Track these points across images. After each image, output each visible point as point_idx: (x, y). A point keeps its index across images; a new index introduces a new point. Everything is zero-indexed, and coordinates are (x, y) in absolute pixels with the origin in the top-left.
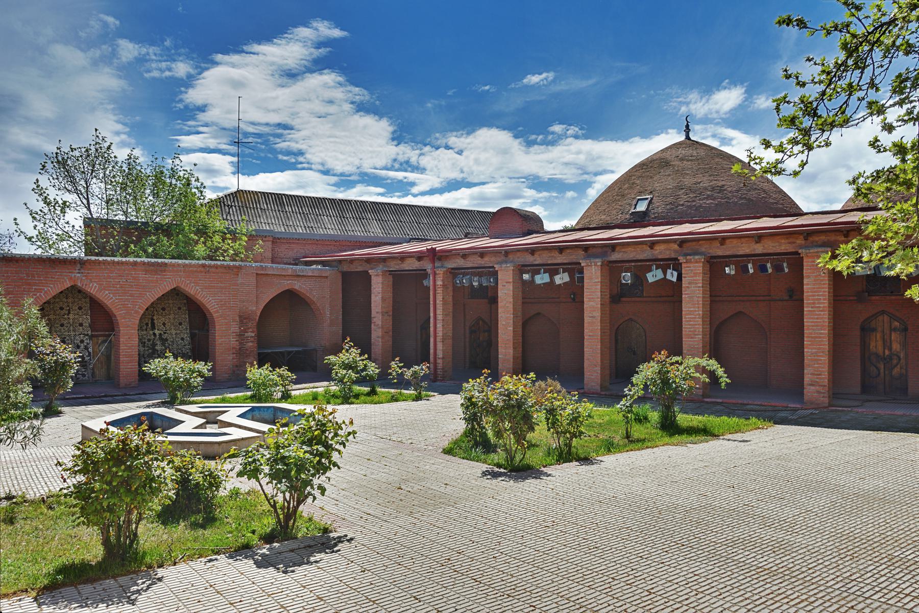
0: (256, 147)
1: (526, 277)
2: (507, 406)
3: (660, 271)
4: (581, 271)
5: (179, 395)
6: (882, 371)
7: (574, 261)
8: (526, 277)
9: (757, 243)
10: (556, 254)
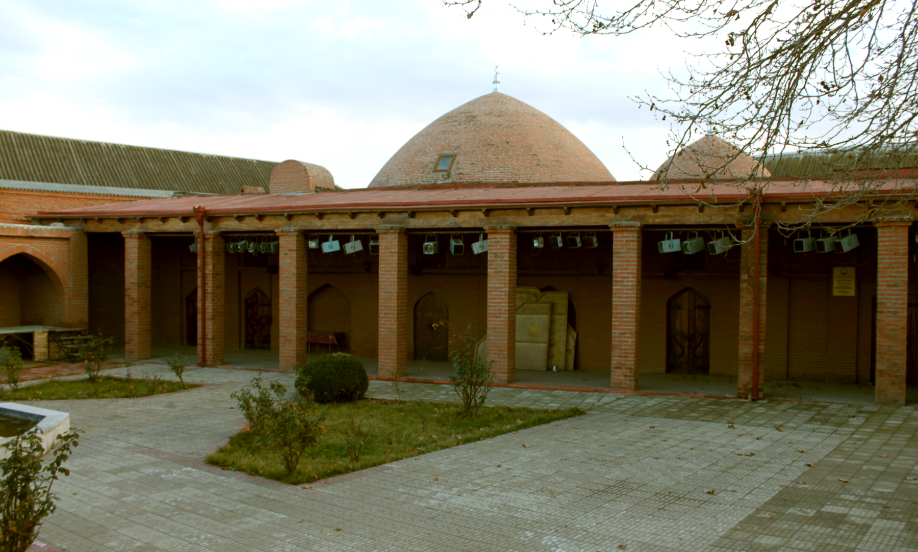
1: (313, 245)
4: (376, 238)
6: (686, 349)
7: (369, 227)
8: (313, 245)
10: (347, 219)
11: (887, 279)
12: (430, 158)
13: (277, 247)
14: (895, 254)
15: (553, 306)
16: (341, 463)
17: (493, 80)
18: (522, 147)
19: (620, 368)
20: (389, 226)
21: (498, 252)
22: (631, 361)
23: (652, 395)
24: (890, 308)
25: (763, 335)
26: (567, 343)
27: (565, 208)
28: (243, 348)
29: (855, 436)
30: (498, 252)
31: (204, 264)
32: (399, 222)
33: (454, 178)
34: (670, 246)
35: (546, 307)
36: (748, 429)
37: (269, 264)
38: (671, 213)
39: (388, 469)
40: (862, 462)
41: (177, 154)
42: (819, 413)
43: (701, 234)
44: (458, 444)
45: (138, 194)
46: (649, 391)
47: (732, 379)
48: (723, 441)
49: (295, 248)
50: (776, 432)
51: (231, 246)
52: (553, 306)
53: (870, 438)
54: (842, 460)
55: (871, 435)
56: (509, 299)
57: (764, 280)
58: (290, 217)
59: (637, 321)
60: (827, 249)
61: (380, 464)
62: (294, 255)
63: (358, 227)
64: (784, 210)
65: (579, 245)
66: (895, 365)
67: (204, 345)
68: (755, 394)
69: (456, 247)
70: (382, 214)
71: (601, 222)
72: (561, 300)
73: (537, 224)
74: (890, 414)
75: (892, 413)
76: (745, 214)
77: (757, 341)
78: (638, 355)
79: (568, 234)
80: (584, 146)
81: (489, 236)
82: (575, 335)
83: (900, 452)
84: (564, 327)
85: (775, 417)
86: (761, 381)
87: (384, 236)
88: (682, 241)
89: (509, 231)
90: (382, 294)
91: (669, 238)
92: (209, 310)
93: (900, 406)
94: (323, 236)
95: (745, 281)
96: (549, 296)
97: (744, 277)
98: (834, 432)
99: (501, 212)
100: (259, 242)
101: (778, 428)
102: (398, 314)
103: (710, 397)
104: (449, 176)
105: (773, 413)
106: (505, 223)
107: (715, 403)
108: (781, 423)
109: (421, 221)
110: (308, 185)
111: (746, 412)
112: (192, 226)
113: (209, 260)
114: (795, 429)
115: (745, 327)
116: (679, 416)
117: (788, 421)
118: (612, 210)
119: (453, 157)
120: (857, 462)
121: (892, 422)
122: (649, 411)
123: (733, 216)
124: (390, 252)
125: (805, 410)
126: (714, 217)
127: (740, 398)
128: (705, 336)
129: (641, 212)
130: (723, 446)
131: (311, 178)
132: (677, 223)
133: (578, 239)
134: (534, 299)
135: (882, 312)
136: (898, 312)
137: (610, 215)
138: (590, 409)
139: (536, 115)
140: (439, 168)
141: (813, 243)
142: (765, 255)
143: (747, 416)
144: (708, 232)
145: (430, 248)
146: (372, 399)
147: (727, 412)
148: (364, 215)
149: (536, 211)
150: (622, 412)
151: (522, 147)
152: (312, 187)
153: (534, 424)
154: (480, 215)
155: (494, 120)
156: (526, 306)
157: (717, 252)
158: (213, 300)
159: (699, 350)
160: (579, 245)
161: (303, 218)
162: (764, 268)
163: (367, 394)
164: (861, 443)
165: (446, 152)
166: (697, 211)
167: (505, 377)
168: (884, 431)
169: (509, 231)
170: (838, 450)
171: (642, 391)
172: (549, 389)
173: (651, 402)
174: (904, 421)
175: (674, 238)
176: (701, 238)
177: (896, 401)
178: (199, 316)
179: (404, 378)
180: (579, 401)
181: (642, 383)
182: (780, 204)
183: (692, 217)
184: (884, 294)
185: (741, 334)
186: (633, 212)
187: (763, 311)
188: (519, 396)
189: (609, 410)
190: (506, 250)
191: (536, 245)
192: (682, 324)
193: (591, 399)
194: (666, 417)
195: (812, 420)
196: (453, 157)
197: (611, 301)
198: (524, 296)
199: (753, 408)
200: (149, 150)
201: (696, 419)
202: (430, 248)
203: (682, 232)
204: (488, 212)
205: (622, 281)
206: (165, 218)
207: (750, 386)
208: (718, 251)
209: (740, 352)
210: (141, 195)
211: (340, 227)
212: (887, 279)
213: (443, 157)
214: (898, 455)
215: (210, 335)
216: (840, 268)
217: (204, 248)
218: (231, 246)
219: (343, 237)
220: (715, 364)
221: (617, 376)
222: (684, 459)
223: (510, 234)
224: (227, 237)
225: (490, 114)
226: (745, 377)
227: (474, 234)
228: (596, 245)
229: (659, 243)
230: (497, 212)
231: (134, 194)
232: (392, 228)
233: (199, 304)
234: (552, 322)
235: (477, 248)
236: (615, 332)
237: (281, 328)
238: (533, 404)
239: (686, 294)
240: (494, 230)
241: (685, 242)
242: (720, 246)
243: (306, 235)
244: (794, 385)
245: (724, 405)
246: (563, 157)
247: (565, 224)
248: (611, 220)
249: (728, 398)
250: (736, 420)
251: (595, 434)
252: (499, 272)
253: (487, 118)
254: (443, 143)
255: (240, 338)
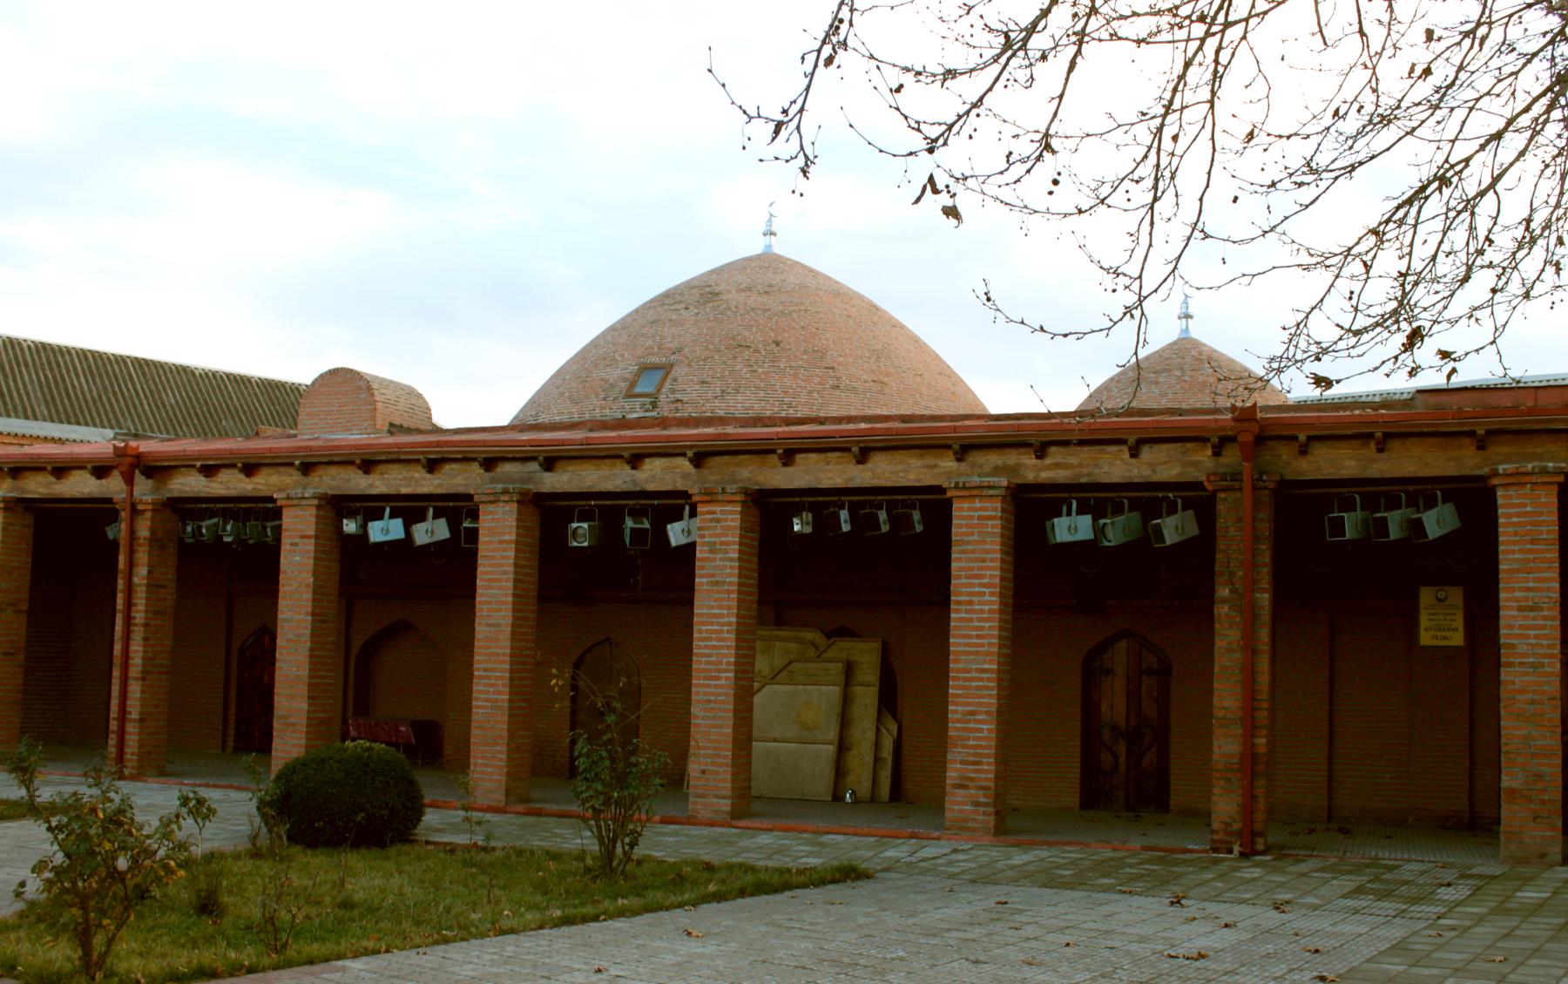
0: (200, 810)
1: (350, 527)
2: (57, 874)
3: (442, 522)
4: (474, 515)
5: (631, 827)
6: (1122, 759)
7: (461, 490)
8: (350, 527)
9: (859, 462)
10: (419, 473)
11: (1517, 594)
12: (623, 370)
13: (278, 531)
14: (1533, 542)
15: (849, 668)
16: (247, 956)
17: (763, 228)
18: (805, 352)
19: (965, 787)
20: (500, 487)
21: (717, 542)
22: (987, 772)
23: (1032, 844)
24: (1526, 655)
25: (1263, 716)
26: (877, 745)
27: (855, 449)
28: (229, 750)
29: (1443, 921)
30: (717, 542)
31: (131, 565)
32: (522, 481)
33: (665, 410)
34: (1071, 528)
35: (836, 669)
36: (1212, 908)
37: (263, 564)
38: (1072, 460)
39: (344, 969)
40: (1447, 972)
41: (141, 364)
42: (1376, 879)
43: (1135, 505)
44: (541, 927)
45: (35, 433)
46: (1027, 838)
47: (1198, 816)
48: (1145, 931)
49: (312, 533)
50: (1274, 913)
51: (189, 529)
52: (849, 668)
53: (1475, 925)
54: (1401, 968)
55: (1480, 920)
56: (738, 640)
57: (1264, 598)
58: (307, 468)
59: (999, 687)
60: (1394, 533)
61: (327, 960)
62: (310, 546)
63: (439, 491)
64: (1304, 451)
65: (885, 528)
66: (1539, 776)
67: (122, 733)
68: (1250, 842)
69: (632, 530)
70: (489, 464)
71: (927, 479)
72: (866, 655)
73: (798, 483)
74: (1525, 881)
75: (1532, 879)
76: (1222, 460)
77: (1251, 729)
78: (1002, 760)
79: (862, 504)
80: (937, 358)
81: (700, 509)
82: (894, 728)
83: (1535, 952)
84: (873, 711)
85: (1280, 885)
86: (1260, 815)
87: (490, 508)
88: (1095, 520)
89: (739, 497)
90: (481, 630)
91: (1069, 514)
92: (137, 661)
93: (1551, 866)
94: (370, 507)
95: (1224, 601)
96: (845, 648)
97: (1223, 592)
98: (1401, 914)
99: (726, 458)
100: (246, 519)
101: (1277, 907)
102: (512, 671)
103: (1153, 849)
104: (654, 405)
105: (1277, 878)
106: (733, 481)
107: (1160, 861)
108: (1289, 896)
109: (565, 477)
110: (374, 418)
111: (1219, 877)
112: (113, 486)
113: (142, 556)
114: (1316, 908)
115: (1226, 698)
116: (1076, 883)
117: (1306, 893)
118: (950, 453)
119: (667, 368)
120: (1435, 971)
121: (1530, 895)
122: (1010, 873)
123: (1198, 464)
124: (500, 541)
125: (1350, 872)
126: (1160, 465)
127: (1215, 850)
128: (1162, 733)
129: (1012, 458)
130: (1142, 940)
131: (379, 405)
132: (1084, 480)
133: (883, 516)
134: (812, 653)
135: (1509, 665)
136: (1543, 665)
137: (948, 463)
138: (887, 870)
139: (840, 293)
140: (637, 390)
141: (1365, 522)
142: (1265, 547)
143: (1219, 884)
144: (1149, 499)
145: (581, 533)
146: (427, 843)
147: (1181, 875)
148: (454, 466)
149: (799, 457)
150: (952, 876)
151: (805, 352)
152: (381, 423)
153: (742, 893)
154: (684, 464)
155: (753, 300)
156: (794, 666)
157: (1168, 542)
158: (145, 639)
159: (1149, 759)
160: (885, 528)
161: (333, 470)
162: (1265, 573)
163: (421, 831)
164: (1454, 933)
165: (655, 360)
166: (1127, 455)
167: (726, 805)
168: (1509, 912)
169: (739, 497)
170: (1398, 948)
171: (1011, 838)
172: (815, 832)
173: (1020, 858)
174: (1554, 893)
175: (1079, 513)
176: (1136, 514)
177: (1543, 856)
178: (116, 673)
179: (521, 808)
180: (870, 854)
181: (1010, 820)
182: (1296, 438)
183: (1115, 467)
184: (1512, 627)
185: (1218, 713)
186: (993, 459)
187: (1264, 663)
188: (746, 843)
189: (925, 872)
190: (733, 538)
191: (797, 528)
192: (1114, 706)
193: (897, 851)
194: (1044, 886)
195: (1359, 891)
196: (667, 368)
197: (947, 645)
198: (793, 646)
199: (1237, 869)
200: (83, 354)
201: (1107, 889)
202: (581, 533)
203: (1097, 499)
204: (699, 459)
205: (970, 603)
206: (60, 469)
207: (1237, 826)
208: (1170, 537)
209: (1216, 751)
210: (42, 434)
211: (404, 491)
212: (1517, 594)
213: (645, 369)
214: (1529, 957)
215: (134, 713)
216: (1433, 589)
217: (132, 531)
218: (189, 529)
219: (410, 509)
220: (1180, 790)
221: (959, 804)
222: (1040, 964)
223: (743, 503)
224: (184, 508)
225: (749, 289)
226: (1225, 807)
227: (674, 505)
228: (919, 528)
229: (1048, 524)
230: (718, 459)
231: (28, 432)
232: (505, 492)
233: (118, 648)
234: (846, 700)
235: (676, 534)
236: (955, 710)
237: (276, 699)
238: (770, 857)
239: (1122, 645)
240: (711, 497)
241: (1102, 521)
242: (1174, 528)
243: (338, 505)
244: (1340, 830)
245: (1177, 863)
246: (888, 374)
247: (856, 483)
248: (948, 475)
249: (1191, 851)
250: (1192, 893)
251: (867, 915)
252: (717, 583)
253: (742, 297)
254: (650, 342)
255: (225, 730)
